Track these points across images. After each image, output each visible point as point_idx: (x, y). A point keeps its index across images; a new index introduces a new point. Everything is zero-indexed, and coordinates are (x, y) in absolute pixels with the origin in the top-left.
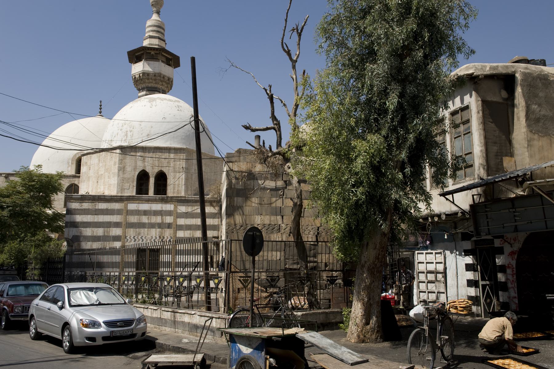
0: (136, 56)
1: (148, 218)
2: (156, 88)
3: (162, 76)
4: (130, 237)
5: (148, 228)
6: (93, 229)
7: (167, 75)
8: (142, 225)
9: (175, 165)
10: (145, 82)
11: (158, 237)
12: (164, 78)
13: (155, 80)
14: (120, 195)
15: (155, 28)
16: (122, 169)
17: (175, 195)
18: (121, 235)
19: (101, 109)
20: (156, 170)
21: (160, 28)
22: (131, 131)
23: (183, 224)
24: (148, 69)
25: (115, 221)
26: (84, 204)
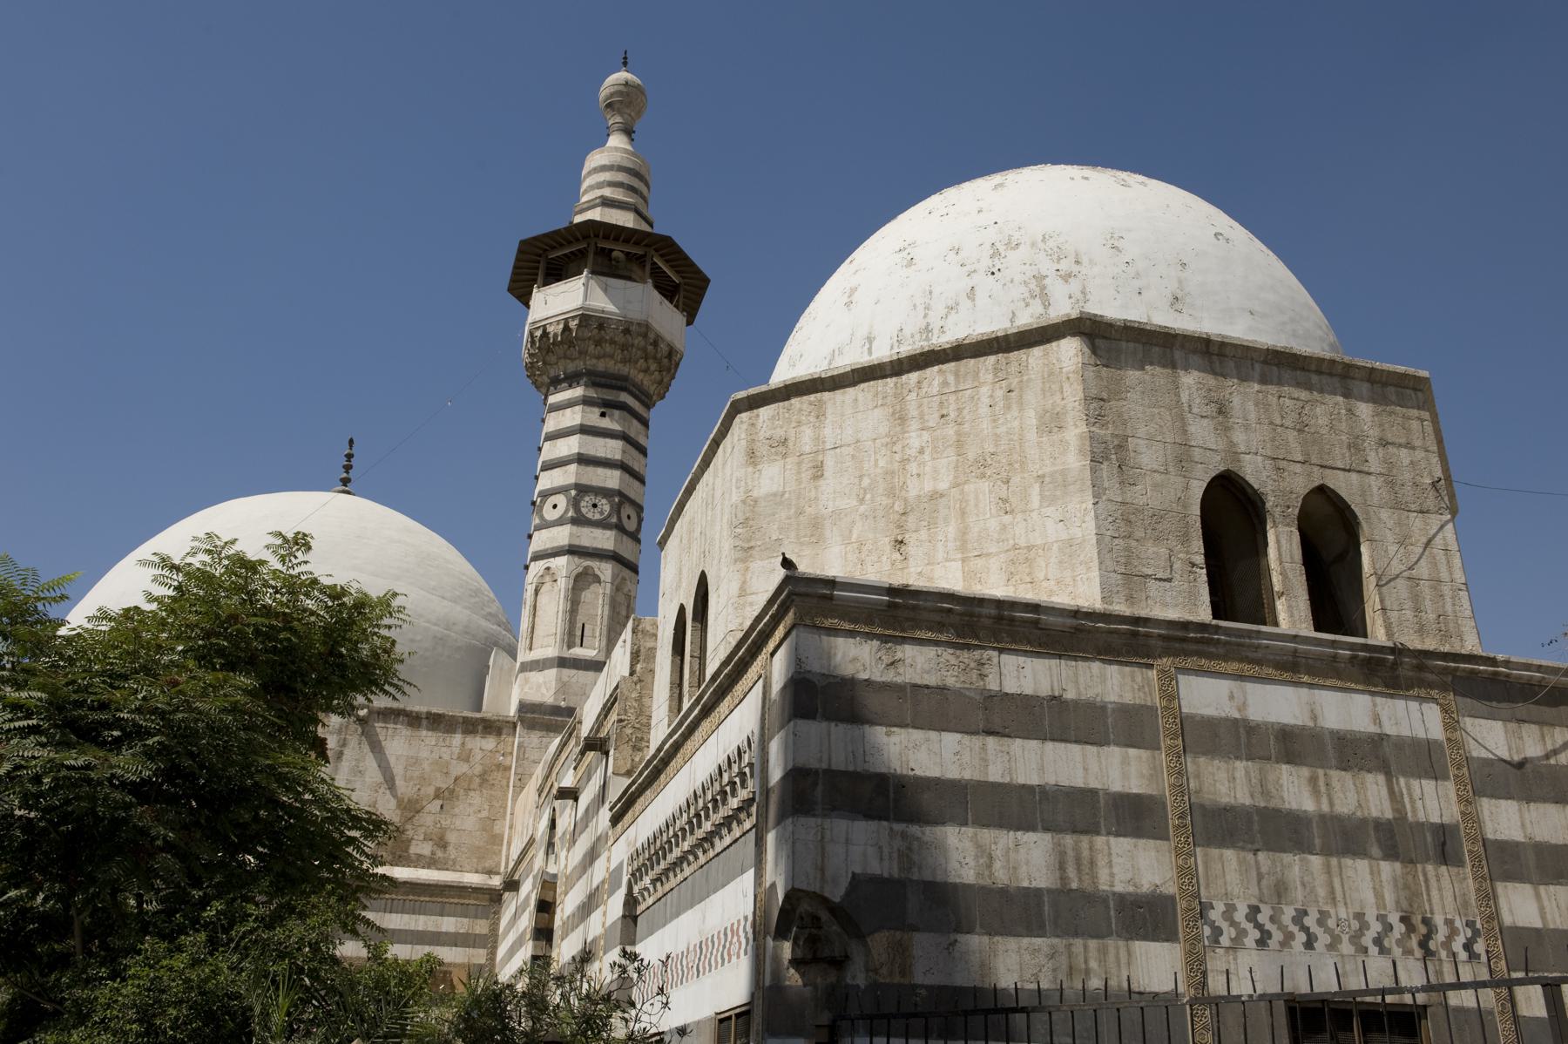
0: (546, 259)
1: (1313, 780)
2: (625, 378)
3: (652, 336)
4: (1230, 909)
5: (1327, 852)
6: (987, 835)
7: (668, 337)
8: (1276, 830)
9: (1390, 464)
10: (583, 353)
11: (1394, 918)
12: (655, 344)
13: (624, 347)
14: (1121, 608)
15: (621, 177)
16: (1109, 454)
17: (1430, 644)
18: (1171, 889)
19: (348, 468)
20: (1300, 483)
21: (636, 179)
22: (1067, 277)
23: (1517, 835)
24: (602, 303)
25: (1116, 787)
26: (908, 652)
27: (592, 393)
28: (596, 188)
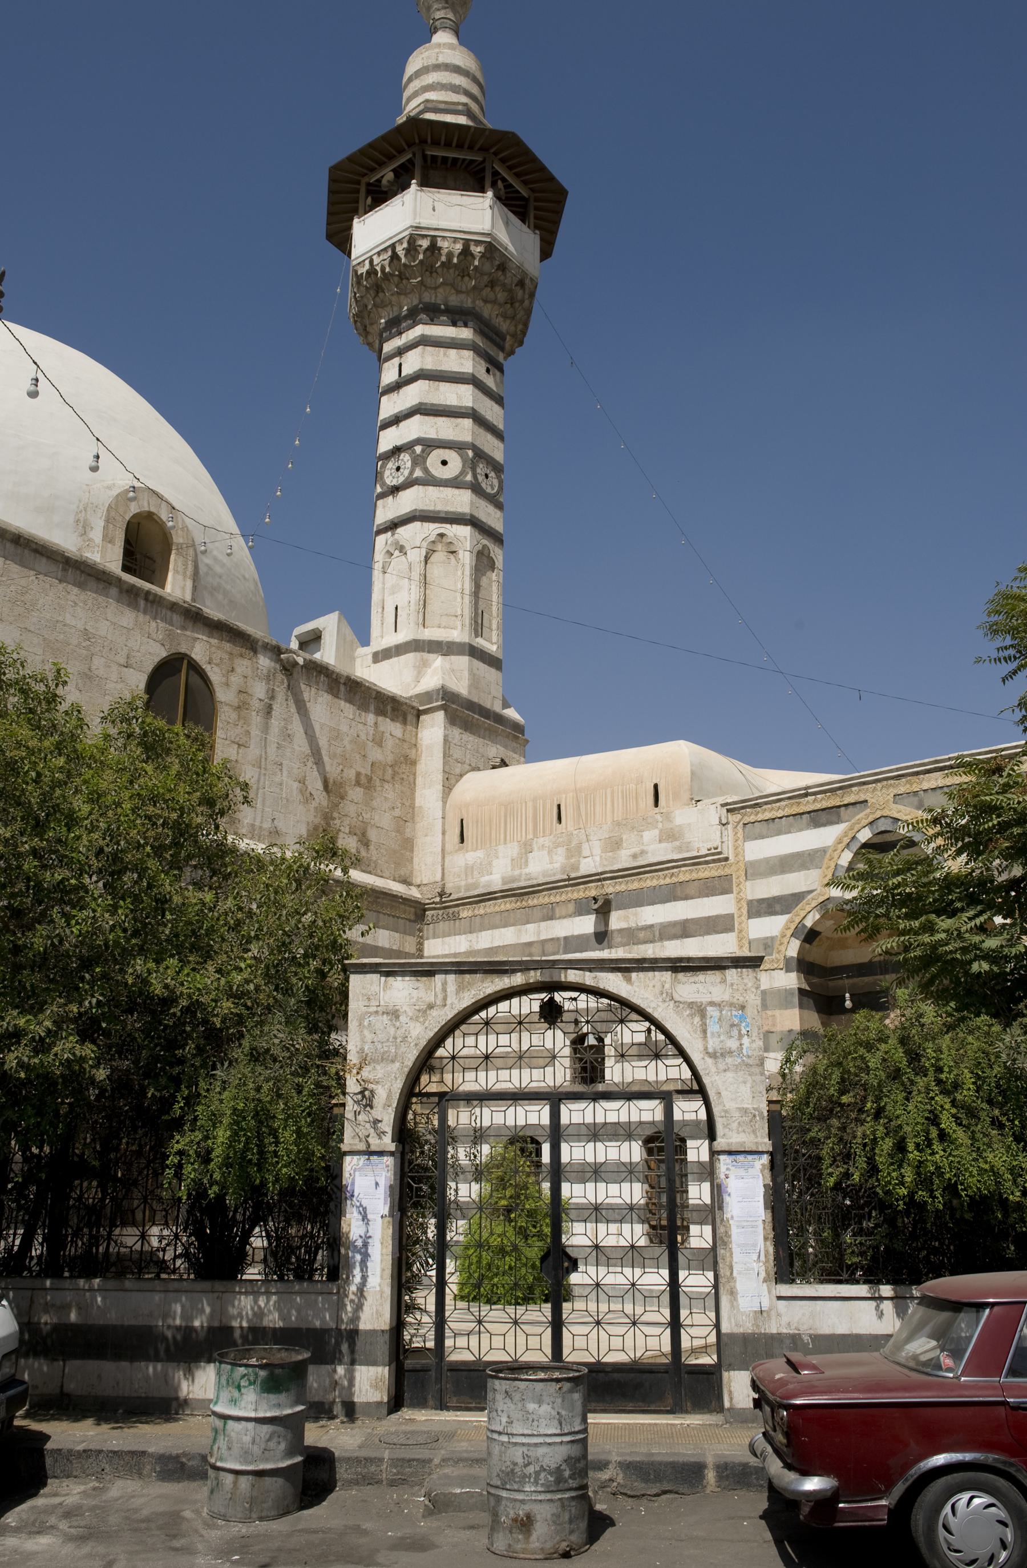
27: (480, 342)
28: (437, 77)
